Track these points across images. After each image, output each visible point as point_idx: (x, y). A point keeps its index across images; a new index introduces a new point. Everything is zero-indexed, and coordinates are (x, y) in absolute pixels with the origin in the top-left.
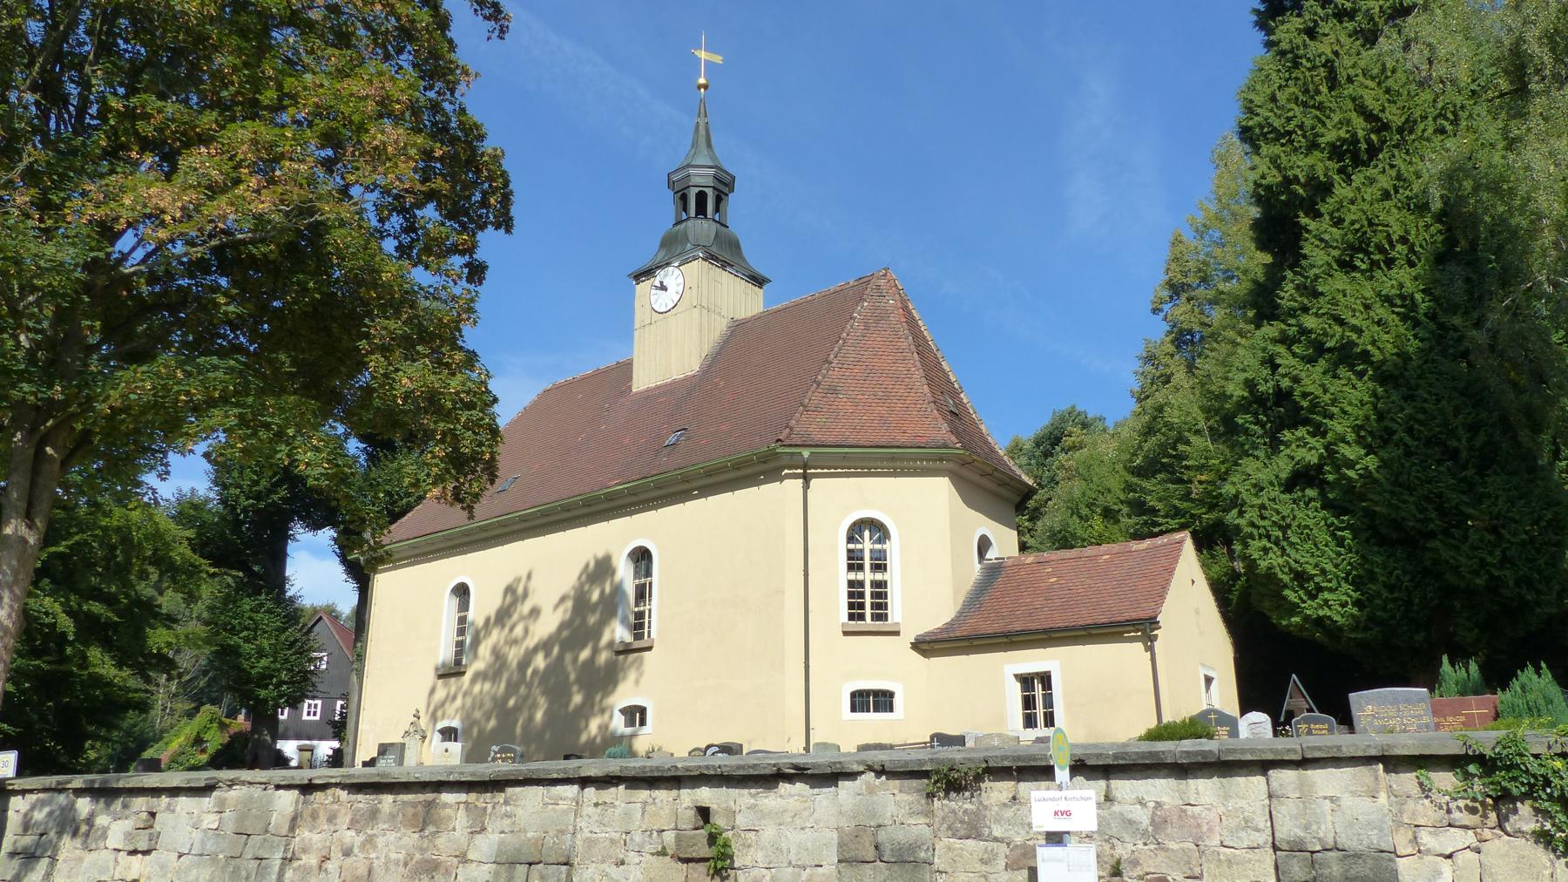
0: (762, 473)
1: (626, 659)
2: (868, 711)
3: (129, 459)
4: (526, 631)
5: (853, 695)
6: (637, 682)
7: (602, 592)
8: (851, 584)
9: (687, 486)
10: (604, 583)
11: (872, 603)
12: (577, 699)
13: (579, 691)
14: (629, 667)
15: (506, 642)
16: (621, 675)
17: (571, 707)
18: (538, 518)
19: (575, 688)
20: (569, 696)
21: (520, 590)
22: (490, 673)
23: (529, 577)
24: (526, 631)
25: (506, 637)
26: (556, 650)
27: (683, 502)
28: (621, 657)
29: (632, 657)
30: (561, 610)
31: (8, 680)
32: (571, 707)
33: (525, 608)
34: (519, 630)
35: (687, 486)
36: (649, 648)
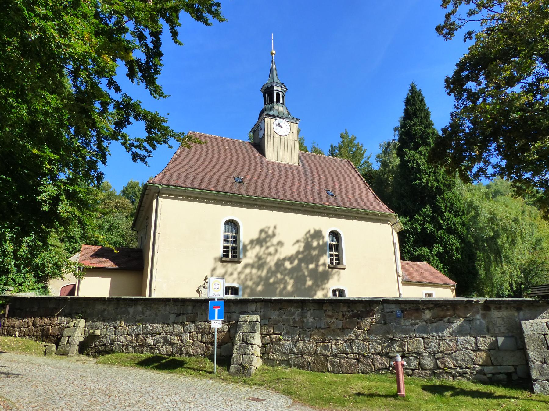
0: (382, 220)
1: (332, 271)
2: (229, 294)
3: (153, 82)
4: (276, 251)
5: (333, 290)
6: (338, 280)
7: (318, 244)
8: (224, 247)
9: (355, 215)
10: (320, 240)
11: (231, 255)
12: (309, 283)
13: (310, 280)
14: (334, 274)
15: (264, 253)
16: (331, 277)
17: (307, 286)
18: (382, 220)
19: (308, 279)
20: (306, 281)
21: (270, 232)
22: (256, 265)
23: (275, 227)
24: (276, 251)
25: (264, 251)
26: (296, 262)
27: (308, 215)
28: (330, 270)
29: (335, 271)
30: (297, 246)
31: (303, 238)
32: (307, 286)
33: (275, 241)
34: (272, 250)
35: (355, 215)
36: (344, 269)
